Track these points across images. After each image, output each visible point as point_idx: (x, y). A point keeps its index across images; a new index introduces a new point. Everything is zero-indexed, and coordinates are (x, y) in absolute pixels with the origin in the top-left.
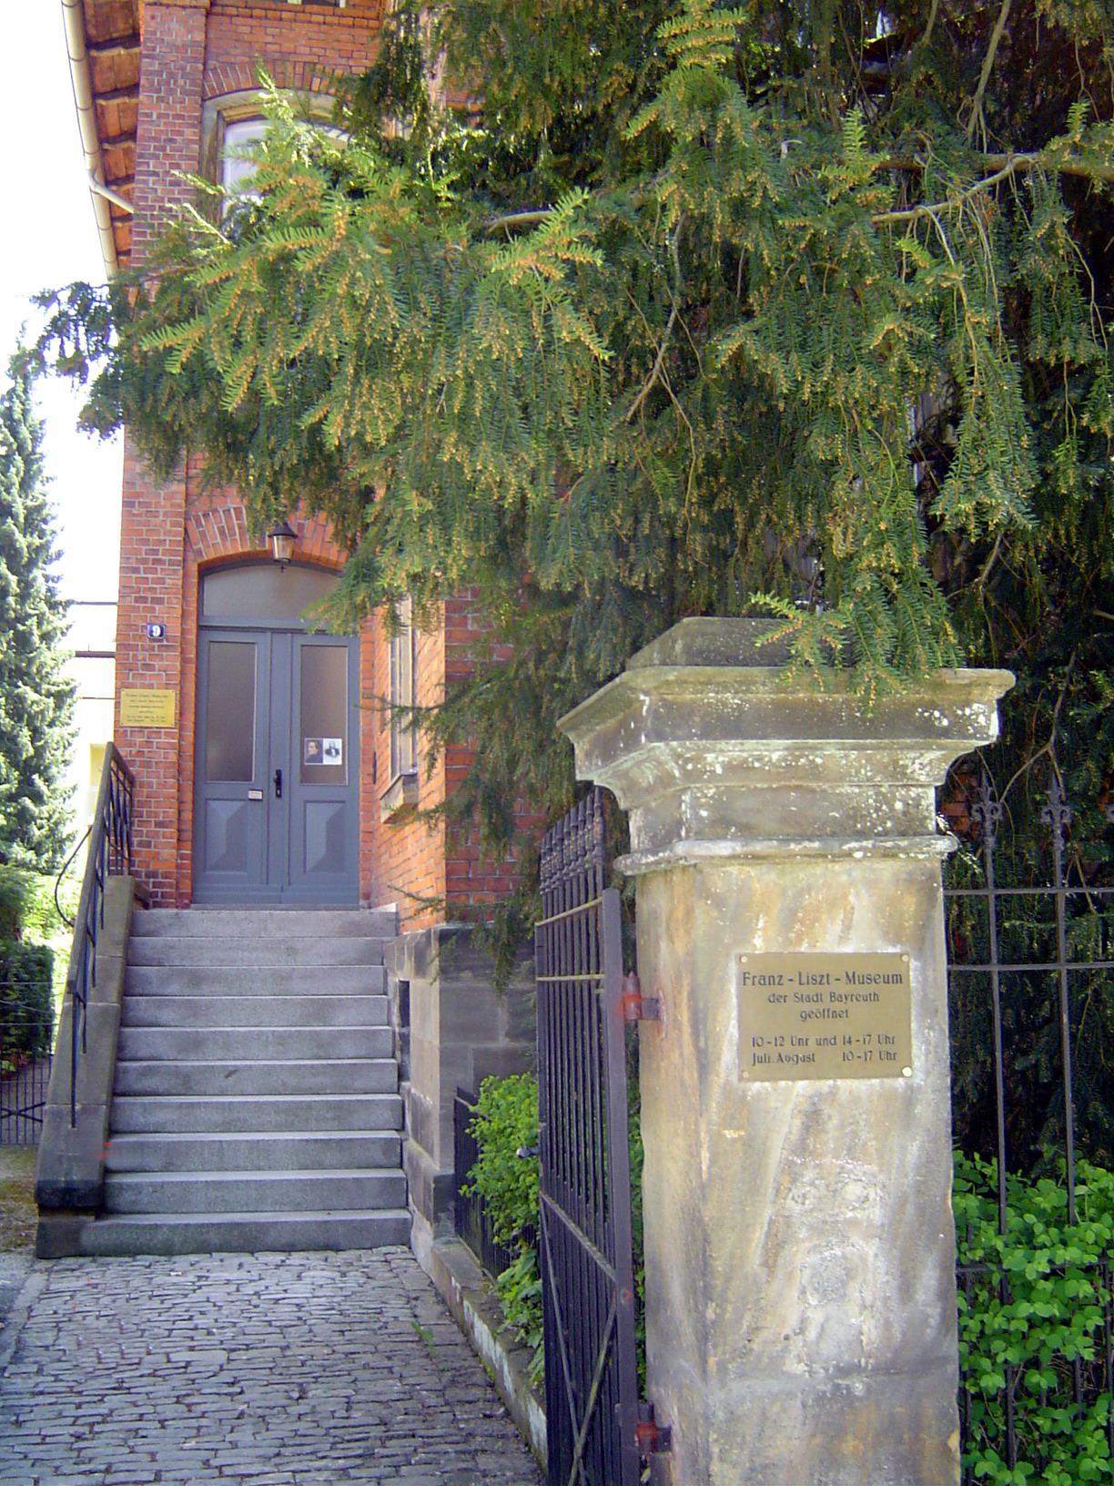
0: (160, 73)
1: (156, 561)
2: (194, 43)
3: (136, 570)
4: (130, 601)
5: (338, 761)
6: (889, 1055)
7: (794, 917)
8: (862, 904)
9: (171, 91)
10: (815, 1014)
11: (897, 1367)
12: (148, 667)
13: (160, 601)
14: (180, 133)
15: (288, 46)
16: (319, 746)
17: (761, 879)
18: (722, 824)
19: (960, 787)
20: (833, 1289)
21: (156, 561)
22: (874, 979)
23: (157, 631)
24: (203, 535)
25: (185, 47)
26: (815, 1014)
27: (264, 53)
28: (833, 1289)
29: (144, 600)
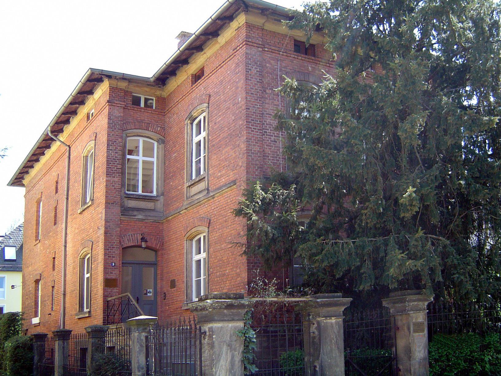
0: (112, 124)
1: (113, 247)
2: (121, 116)
3: (108, 250)
4: (107, 257)
5: (151, 294)
6: (423, 331)
7: (416, 319)
8: (421, 317)
9: (115, 129)
10: (418, 327)
11: (424, 359)
12: (112, 273)
13: (114, 257)
14: (117, 140)
15: (142, 118)
16: (147, 290)
17: (414, 315)
18: (411, 310)
19: (429, 306)
20: (420, 352)
21: (113, 247)
22: (422, 324)
23: (113, 264)
24: (124, 241)
25: (119, 117)
26: (418, 327)
27: (137, 120)
28: (420, 352)
29: (110, 257)
